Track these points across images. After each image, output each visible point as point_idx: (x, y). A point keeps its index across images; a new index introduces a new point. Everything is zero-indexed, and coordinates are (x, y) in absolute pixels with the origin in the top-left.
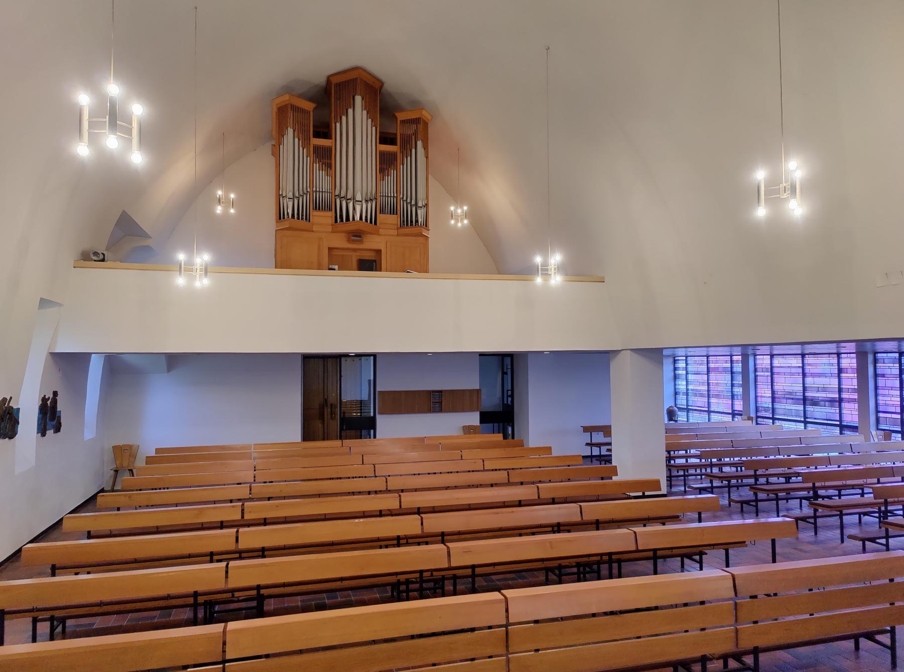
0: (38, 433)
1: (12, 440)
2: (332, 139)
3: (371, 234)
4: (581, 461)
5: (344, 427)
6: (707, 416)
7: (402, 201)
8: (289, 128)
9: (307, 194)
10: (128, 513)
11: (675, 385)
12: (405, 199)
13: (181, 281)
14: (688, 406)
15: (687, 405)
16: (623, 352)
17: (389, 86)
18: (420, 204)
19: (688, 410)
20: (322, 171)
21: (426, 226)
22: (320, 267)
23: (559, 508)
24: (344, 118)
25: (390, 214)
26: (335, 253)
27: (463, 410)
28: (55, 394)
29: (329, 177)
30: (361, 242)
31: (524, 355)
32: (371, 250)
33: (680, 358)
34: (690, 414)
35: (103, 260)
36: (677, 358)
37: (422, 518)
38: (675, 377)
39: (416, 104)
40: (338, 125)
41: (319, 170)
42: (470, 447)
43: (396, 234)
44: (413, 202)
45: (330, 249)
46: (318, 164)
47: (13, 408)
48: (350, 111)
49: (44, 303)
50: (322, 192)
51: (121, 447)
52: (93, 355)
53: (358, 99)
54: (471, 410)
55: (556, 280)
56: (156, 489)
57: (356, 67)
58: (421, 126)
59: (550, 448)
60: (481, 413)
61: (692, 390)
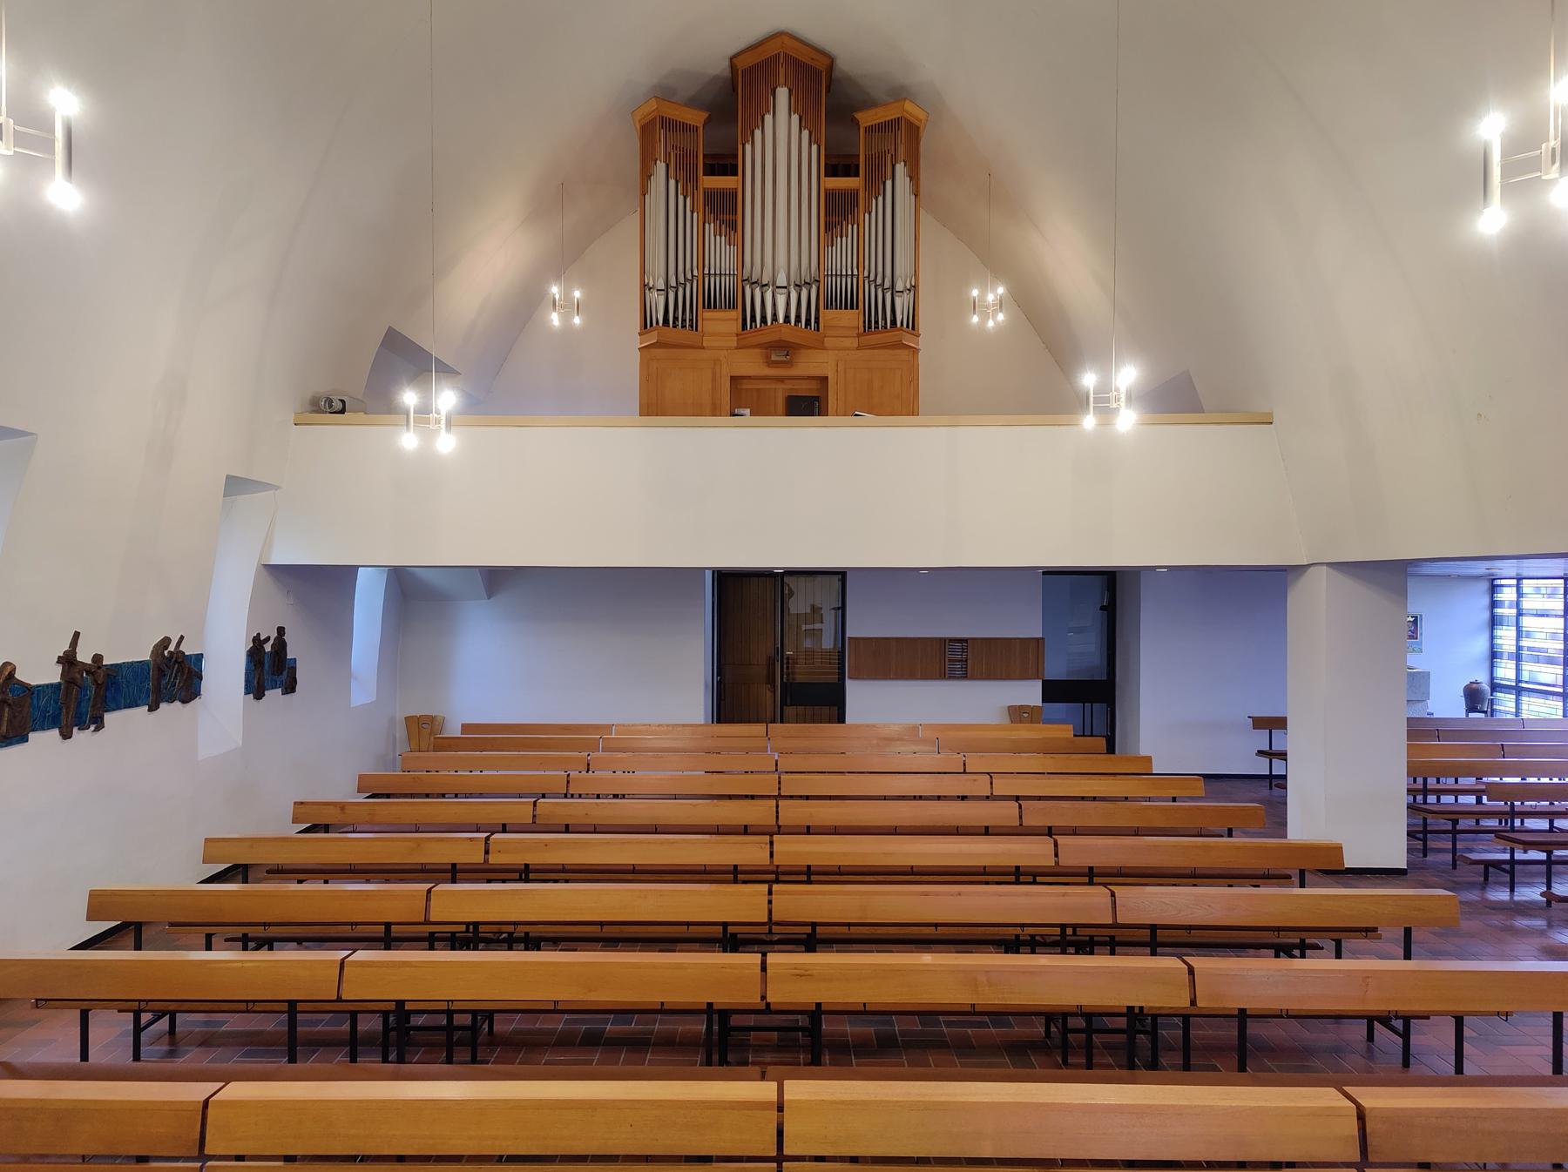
0: (246, 693)
3: (810, 348)
4: (1200, 788)
6: (1561, 704)
7: (866, 282)
8: (658, 162)
9: (692, 281)
11: (1492, 637)
12: (872, 278)
13: (409, 440)
14: (1520, 681)
15: (1518, 680)
16: (1312, 568)
17: (844, 64)
18: (899, 286)
19: (1518, 690)
21: (913, 328)
22: (715, 411)
23: (1064, 895)
24: (758, 133)
26: (746, 385)
27: (1007, 676)
28: (281, 631)
29: (732, 247)
30: (788, 364)
31: (1134, 573)
32: (810, 378)
33: (1503, 582)
34: (1524, 699)
35: (342, 411)
36: (1498, 582)
37: (1056, 845)
38: (1494, 622)
39: (900, 94)
40: (748, 147)
41: (715, 236)
42: (1017, 748)
44: (887, 284)
46: (712, 225)
47: (184, 653)
48: (768, 118)
49: (235, 486)
50: (721, 274)
52: (360, 569)
53: (782, 94)
54: (1024, 676)
55: (1127, 420)
56: (443, 796)
57: (778, 33)
58: (902, 134)
60: (1044, 683)
61: (1529, 649)
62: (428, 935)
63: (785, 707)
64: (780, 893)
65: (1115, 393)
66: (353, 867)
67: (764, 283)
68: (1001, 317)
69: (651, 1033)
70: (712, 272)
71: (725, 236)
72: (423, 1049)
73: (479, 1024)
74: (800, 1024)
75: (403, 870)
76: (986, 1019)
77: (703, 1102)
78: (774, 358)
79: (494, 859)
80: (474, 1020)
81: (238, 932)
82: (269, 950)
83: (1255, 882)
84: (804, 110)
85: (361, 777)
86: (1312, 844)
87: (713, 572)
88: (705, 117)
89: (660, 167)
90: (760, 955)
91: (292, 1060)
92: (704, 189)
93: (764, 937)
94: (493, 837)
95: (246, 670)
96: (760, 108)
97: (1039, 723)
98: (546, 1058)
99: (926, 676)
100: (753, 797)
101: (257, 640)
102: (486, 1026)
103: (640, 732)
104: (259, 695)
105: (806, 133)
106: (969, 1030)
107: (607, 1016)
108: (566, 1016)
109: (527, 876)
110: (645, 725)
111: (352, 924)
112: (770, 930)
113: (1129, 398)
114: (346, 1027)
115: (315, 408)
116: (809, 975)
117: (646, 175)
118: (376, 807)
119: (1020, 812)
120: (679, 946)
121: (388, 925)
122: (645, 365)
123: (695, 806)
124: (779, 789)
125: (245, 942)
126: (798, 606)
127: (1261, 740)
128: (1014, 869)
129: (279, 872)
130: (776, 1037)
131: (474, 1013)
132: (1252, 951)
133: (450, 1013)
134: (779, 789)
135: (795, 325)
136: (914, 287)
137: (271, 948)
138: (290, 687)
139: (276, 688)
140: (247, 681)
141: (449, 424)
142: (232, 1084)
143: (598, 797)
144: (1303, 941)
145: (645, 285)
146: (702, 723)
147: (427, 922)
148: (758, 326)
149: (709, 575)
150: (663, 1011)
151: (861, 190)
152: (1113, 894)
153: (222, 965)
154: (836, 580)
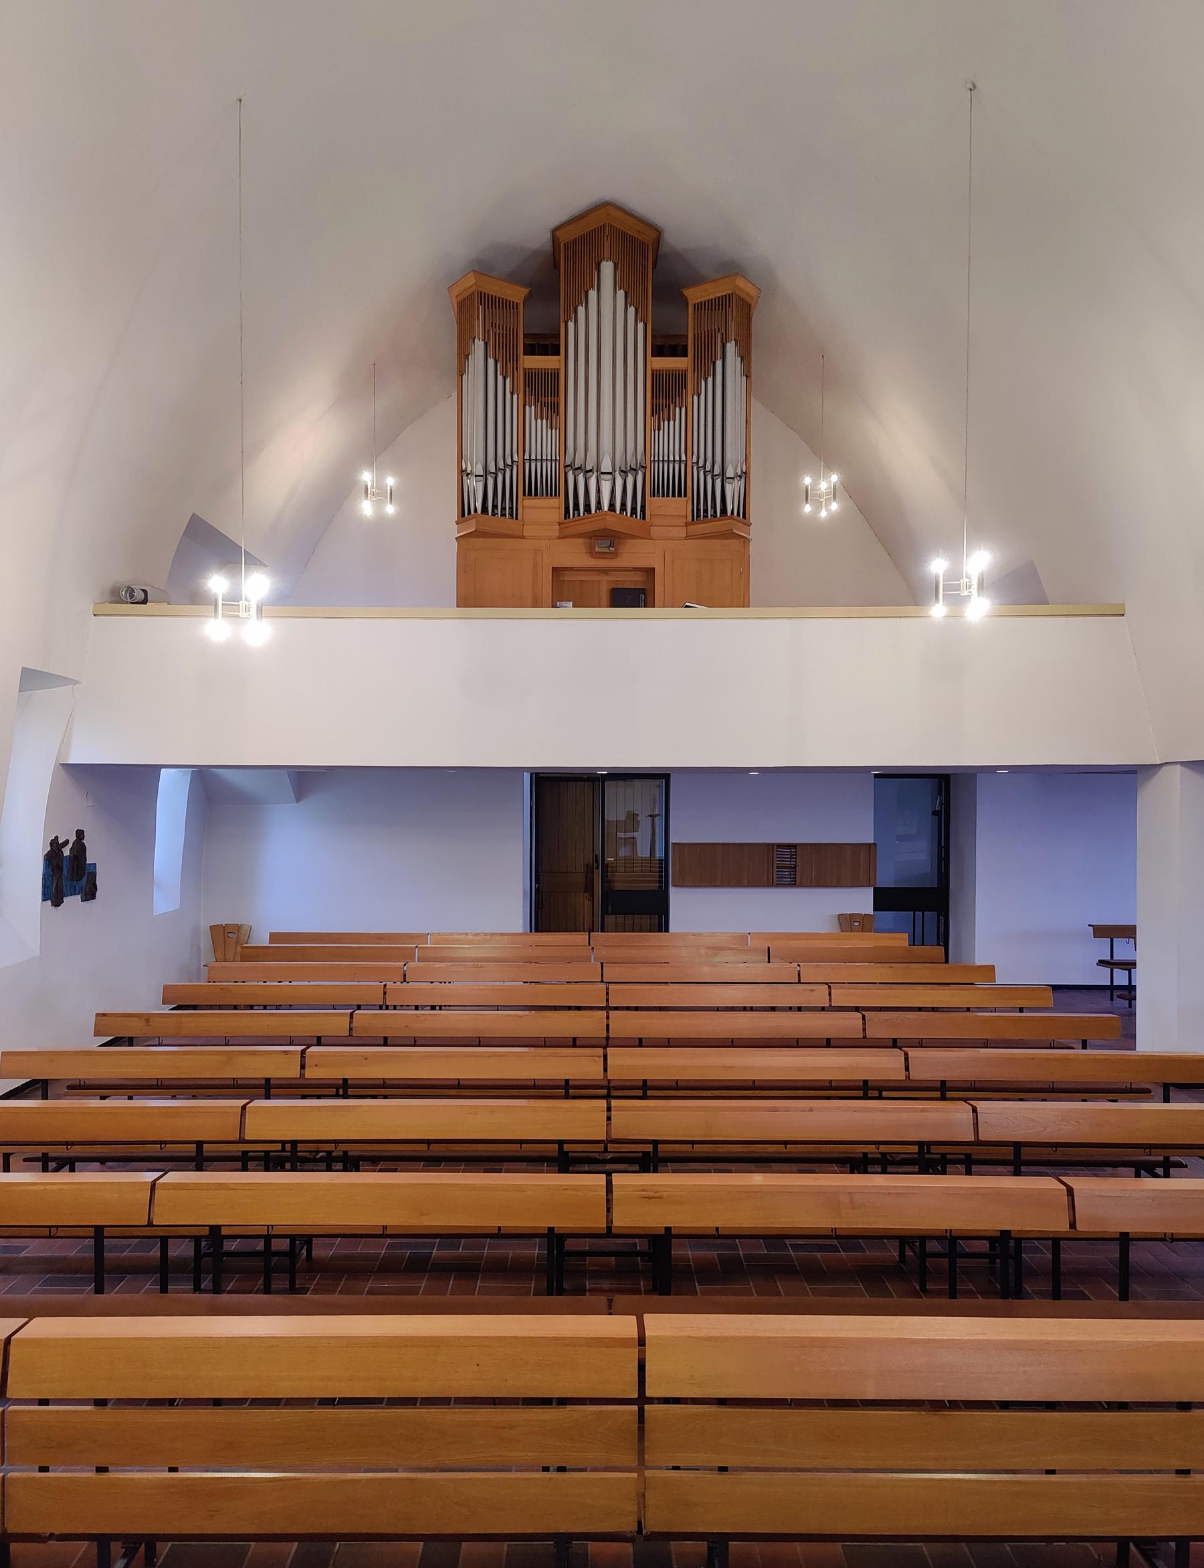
0: (44, 900)
1: (59, 907)
2: (559, 354)
3: (634, 537)
4: (1049, 999)
5: (610, 910)
7: (695, 468)
8: (476, 340)
10: (104, 1052)
12: (701, 463)
16: (1164, 768)
18: (730, 473)
20: (552, 430)
21: (744, 517)
22: (536, 603)
24: (581, 310)
25: (674, 495)
26: (568, 577)
27: (838, 884)
28: (80, 834)
29: (554, 430)
35: (145, 602)
39: (731, 269)
40: (571, 325)
41: (536, 420)
42: (850, 957)
43: (685, 535)
44: (717, 470)
45: (556, 570)
46: (533, 407)
48: (592, 294)
50: (542, 460)
51: (224, 927)
53: (607, 268)
54: (855, 884)
56: (252, 1007)
59: (991, 968)
60: (876, 890)
62: (240, 1154)
63: (606, 916)
64: (620, 1109)
65: (966, 580)
66: (159, 1083)
67: (587, 469)
68: (834, 506)
69: (480, 1257)
70: (533, 457)
71: (547, 420)
72: (238, 1275)
73: (297, 1251)
74: (638, 1248)
75: (414, 1085)
76: (835, 1242)
77: (556, 1339)
78: (597, 550)
79: (311, 1073)
80: (292, 1244)
81: (38, 1151)
82: (70, 1171)
83: (1084, 1096)
84: (628, 284)
85: (166, 988)
86: (1178, 1056)
87: (531, 774)
88: (525, 293)
89: (479, 345)
90: (604, 1175)
91: (99, 1290)
92: (525, 369)
93: (596, 1155)
94: (308, 1050)
95: (44, 875)
96: (588, 281)
97: (870, 932)
98: (369, 1285)
99: (754, 883)
100: (579, 1008)
101: (54, 842)
102: (304, 1252)
103: (447, 941)
104: (57, 903)
105: (632, 310)
106: (818, 1254)
107: (433, 1240)
108: (389, 1240)
109: (345, 1092)
110: (461, 934)
111: (161, 1143)
112: (606, 1148)
113: (981, 585)
114: (156, 1252)
115: (114, 599)
116: (659, 1198)
117: (464, 354)
118: (184, 1019)
119: (864, 1024)
120: (505, 1165)
121: (199, 1144)
122: (463, 555)
123: (520, 1017)
124: (607, 1000)
125: (46, 1163)
126: (615, 811)
127: (1102, 949)
128: (263, 1082)
129: (80, 1088)
130: (614, 1263)
131: (293, 1238)
132: (1109, 1170)
133: (268, 1238)
134: (607, 1000)
135: (620, 513)
136: (744, 473)
137: (72, 1170)
138: (90, 894)
139: (75, 894)
140: (45, 887)
141: (260, 610)
142: (36, 1320)
143: (417, 1008)
144: (1167, 1158)
145: (463, 471)
146: (521, 932)
147: (242, 1141)
148: (582, 515)
149: (527, 776)
150: (499, 1235)
151: (690, 370)
152: (975, 1110)
153: (25, 1188)
154: (654, 788)
